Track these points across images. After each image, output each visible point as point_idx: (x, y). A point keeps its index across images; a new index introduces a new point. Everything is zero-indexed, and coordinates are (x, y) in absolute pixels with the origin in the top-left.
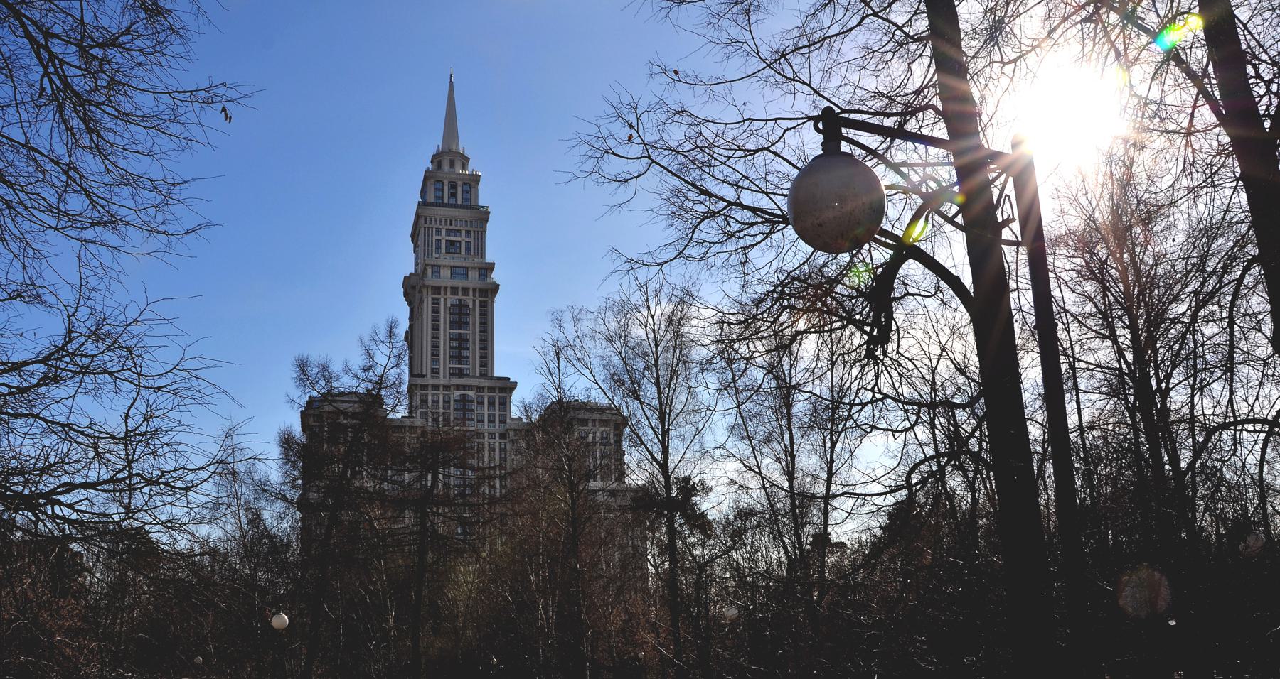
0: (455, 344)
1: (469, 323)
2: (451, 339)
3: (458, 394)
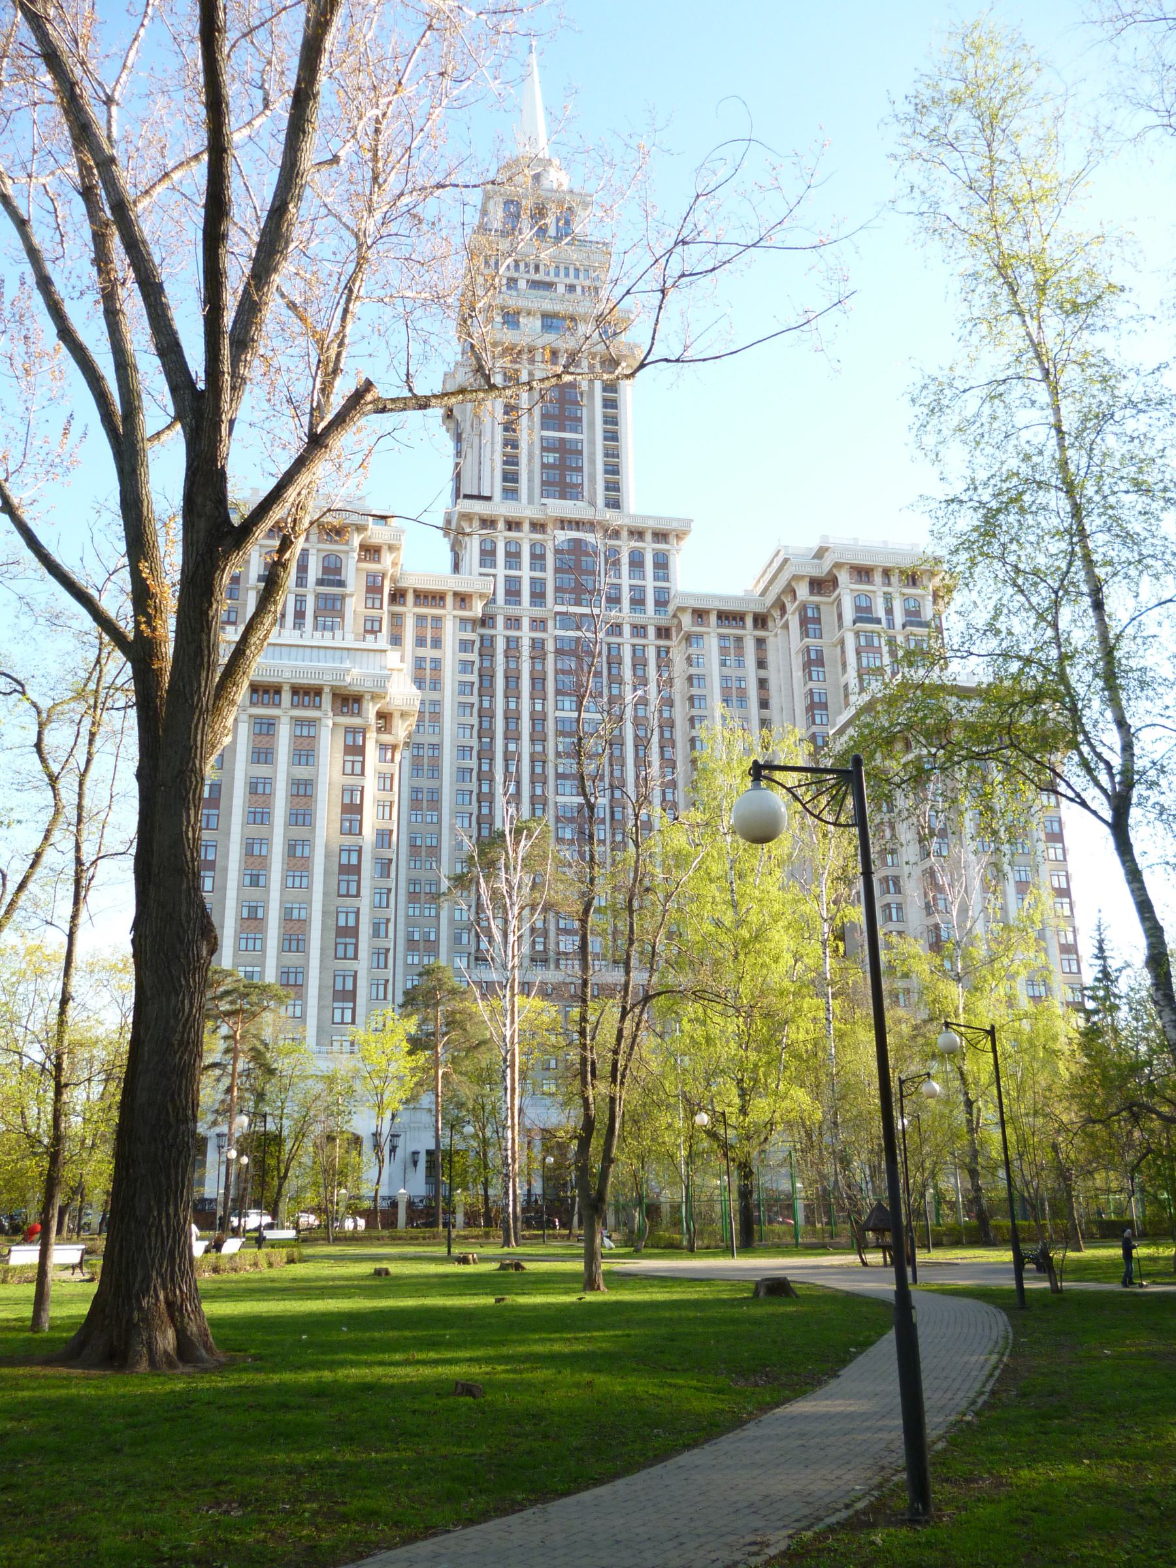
0: (551, 458)
1: (580, 420)
2: (543, 449)
3: (563, 536)
